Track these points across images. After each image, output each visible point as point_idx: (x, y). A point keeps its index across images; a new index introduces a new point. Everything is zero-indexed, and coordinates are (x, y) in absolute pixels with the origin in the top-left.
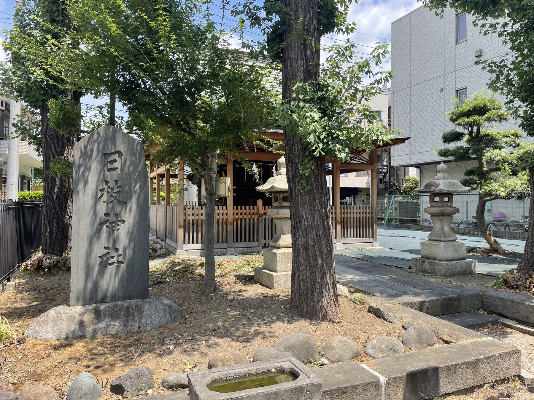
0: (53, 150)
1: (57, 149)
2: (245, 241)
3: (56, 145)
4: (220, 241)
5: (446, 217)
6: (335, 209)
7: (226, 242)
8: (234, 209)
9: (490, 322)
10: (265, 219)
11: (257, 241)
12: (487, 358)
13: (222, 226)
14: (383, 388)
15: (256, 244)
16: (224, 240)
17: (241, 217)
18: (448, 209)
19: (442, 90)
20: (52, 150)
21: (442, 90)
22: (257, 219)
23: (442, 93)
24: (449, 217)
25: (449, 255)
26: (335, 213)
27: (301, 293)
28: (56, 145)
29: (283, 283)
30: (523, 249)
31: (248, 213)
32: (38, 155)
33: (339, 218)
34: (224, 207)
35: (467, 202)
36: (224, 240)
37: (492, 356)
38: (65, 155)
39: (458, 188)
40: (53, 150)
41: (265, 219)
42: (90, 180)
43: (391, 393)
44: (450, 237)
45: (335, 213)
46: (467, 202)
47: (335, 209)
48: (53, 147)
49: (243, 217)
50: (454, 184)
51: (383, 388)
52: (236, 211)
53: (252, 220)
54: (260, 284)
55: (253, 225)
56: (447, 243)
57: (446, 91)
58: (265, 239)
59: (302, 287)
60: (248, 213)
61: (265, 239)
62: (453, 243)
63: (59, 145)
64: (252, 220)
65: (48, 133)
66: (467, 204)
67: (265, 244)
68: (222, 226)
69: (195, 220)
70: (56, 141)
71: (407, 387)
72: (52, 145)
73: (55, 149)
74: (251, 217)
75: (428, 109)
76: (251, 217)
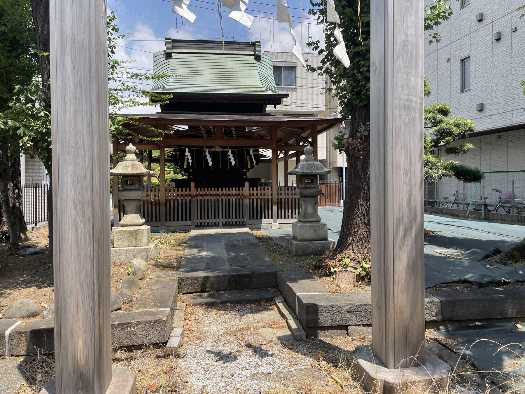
2: (178, 220)
4: (168, 219)
5: (308, 199)
6: (272, 190)
7: (160, 220)
8: (250, 190)
9: (265, 299)
10: (197, 200)
11: (190, 220)
12: (123, 324)
13: (156, 207)
14: (7, 339)
15: (189, 223)
17: (257, 197)
18: (308, 190)
19: (449, 60)
21: (449, 60)
22: (190, 200)
23: (449, 64)
24: (312, 199)
25: (307, 235)
26: (272, 194)
31: (180, 195)
33: (275, 200)
34: (188, 189)
35: (513, 181)
37: (128, 323)
39: (318, 170)
41: (197, 200)
43: (14, 343)
44: (312, 218)
45: (272, 194)
47: (272, 190)
49: (176, 198)
50: (314, 166)
51: (7, 339)
52: (252, 192)
53: (184, 201)
55: (178, 205)
56: (305, 224)
57: (452, 61)
58: (198, 219)
60: (180, 195)
61: (198, 219)
62: (316, 224)
64: (184, 201)
66: (513, 183)
67: (198, 223)
68: (156, 207)
69: (266, 199)
71: (30, 341)
74: (184, 198)
75: (436, 81)
76: (184, 198)
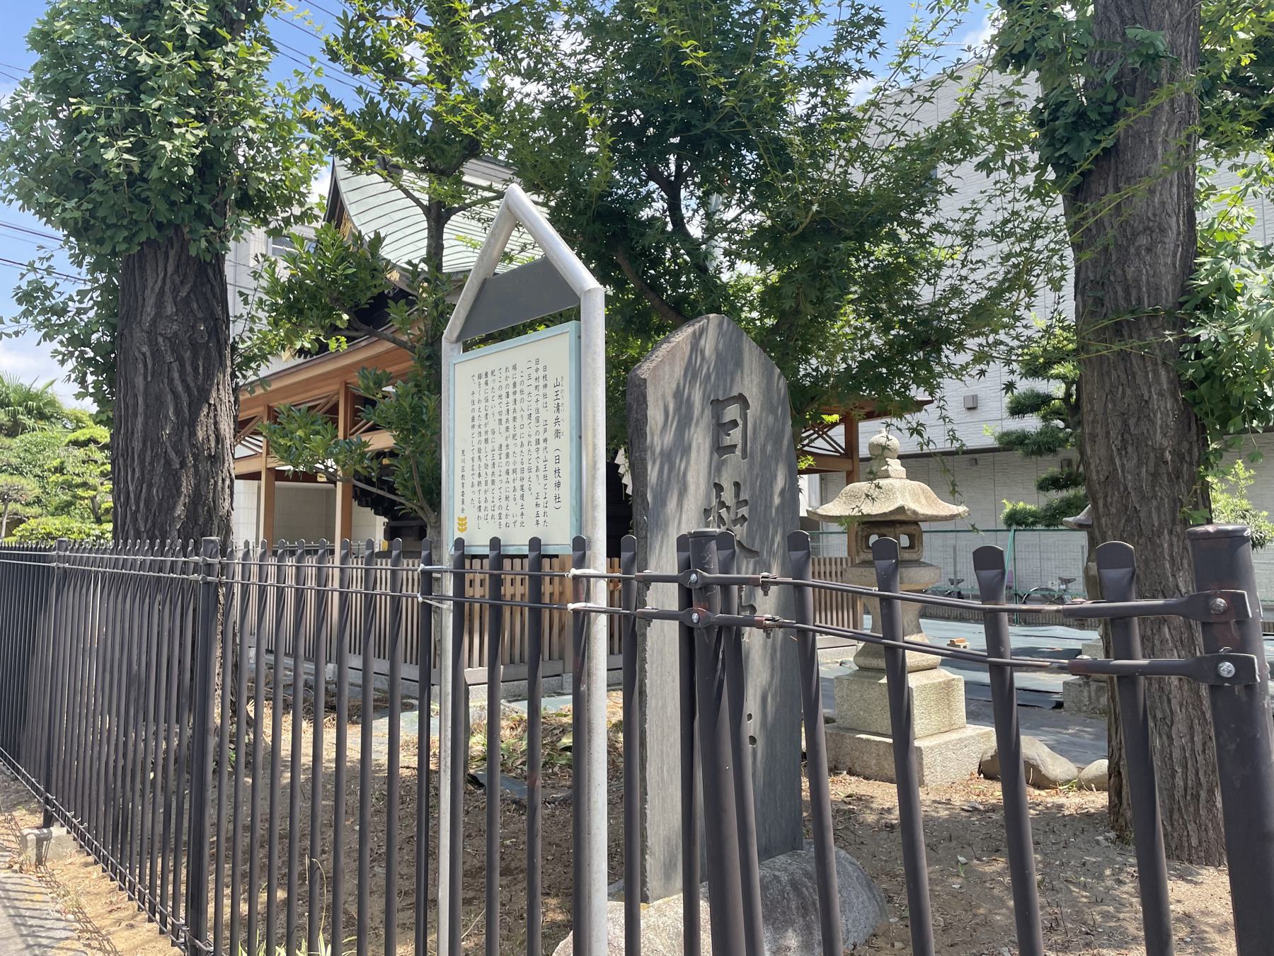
0: (177, 382)
1: (190, 379)
3: (189, 369)
7: (561, 658)
16: (556, 655)
20: (171, 381)
27: (1178, 795)
28: (189, 369)
29: (938, 769)
30: (818, 645)
32: (79, 396)
35: (955, 548)
36: (556, 655)
38: (212, 402)
40: (177, 382)
42: (691, 478)
46: (955, 548)
48: (176, 375)
54: (851, 773)
59: (1179, 782)
63: (196, 369)
65: (161, 329)
70: (188, 355)
72: (175, 366)
73: (183, 381)
